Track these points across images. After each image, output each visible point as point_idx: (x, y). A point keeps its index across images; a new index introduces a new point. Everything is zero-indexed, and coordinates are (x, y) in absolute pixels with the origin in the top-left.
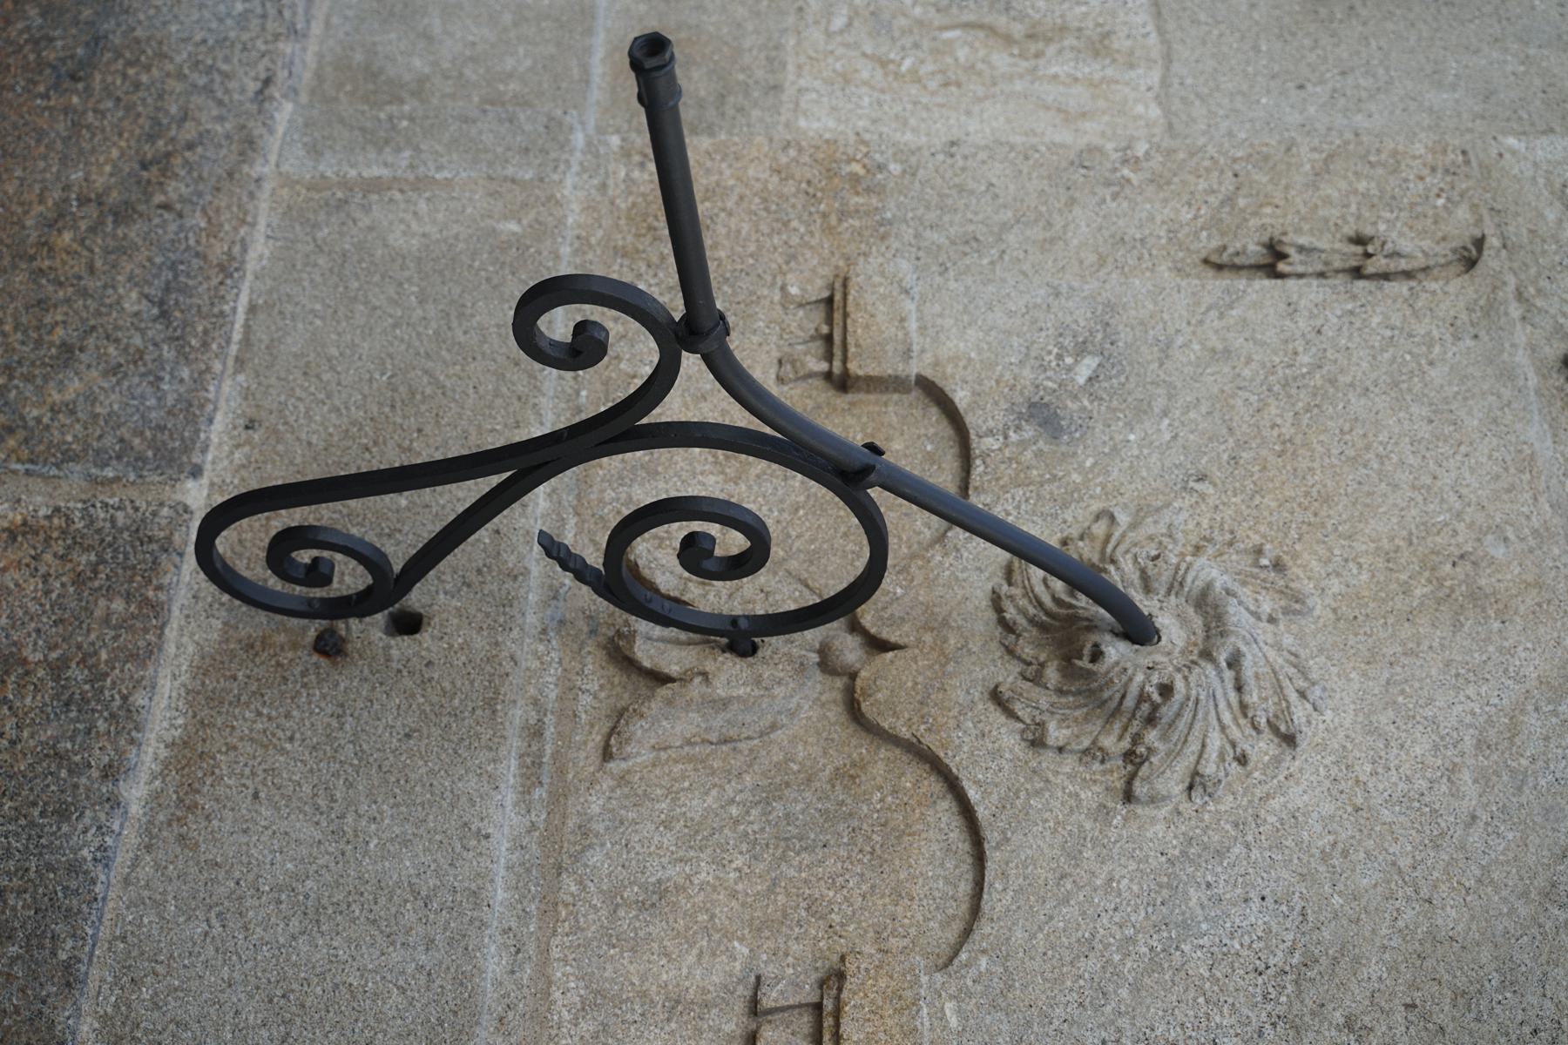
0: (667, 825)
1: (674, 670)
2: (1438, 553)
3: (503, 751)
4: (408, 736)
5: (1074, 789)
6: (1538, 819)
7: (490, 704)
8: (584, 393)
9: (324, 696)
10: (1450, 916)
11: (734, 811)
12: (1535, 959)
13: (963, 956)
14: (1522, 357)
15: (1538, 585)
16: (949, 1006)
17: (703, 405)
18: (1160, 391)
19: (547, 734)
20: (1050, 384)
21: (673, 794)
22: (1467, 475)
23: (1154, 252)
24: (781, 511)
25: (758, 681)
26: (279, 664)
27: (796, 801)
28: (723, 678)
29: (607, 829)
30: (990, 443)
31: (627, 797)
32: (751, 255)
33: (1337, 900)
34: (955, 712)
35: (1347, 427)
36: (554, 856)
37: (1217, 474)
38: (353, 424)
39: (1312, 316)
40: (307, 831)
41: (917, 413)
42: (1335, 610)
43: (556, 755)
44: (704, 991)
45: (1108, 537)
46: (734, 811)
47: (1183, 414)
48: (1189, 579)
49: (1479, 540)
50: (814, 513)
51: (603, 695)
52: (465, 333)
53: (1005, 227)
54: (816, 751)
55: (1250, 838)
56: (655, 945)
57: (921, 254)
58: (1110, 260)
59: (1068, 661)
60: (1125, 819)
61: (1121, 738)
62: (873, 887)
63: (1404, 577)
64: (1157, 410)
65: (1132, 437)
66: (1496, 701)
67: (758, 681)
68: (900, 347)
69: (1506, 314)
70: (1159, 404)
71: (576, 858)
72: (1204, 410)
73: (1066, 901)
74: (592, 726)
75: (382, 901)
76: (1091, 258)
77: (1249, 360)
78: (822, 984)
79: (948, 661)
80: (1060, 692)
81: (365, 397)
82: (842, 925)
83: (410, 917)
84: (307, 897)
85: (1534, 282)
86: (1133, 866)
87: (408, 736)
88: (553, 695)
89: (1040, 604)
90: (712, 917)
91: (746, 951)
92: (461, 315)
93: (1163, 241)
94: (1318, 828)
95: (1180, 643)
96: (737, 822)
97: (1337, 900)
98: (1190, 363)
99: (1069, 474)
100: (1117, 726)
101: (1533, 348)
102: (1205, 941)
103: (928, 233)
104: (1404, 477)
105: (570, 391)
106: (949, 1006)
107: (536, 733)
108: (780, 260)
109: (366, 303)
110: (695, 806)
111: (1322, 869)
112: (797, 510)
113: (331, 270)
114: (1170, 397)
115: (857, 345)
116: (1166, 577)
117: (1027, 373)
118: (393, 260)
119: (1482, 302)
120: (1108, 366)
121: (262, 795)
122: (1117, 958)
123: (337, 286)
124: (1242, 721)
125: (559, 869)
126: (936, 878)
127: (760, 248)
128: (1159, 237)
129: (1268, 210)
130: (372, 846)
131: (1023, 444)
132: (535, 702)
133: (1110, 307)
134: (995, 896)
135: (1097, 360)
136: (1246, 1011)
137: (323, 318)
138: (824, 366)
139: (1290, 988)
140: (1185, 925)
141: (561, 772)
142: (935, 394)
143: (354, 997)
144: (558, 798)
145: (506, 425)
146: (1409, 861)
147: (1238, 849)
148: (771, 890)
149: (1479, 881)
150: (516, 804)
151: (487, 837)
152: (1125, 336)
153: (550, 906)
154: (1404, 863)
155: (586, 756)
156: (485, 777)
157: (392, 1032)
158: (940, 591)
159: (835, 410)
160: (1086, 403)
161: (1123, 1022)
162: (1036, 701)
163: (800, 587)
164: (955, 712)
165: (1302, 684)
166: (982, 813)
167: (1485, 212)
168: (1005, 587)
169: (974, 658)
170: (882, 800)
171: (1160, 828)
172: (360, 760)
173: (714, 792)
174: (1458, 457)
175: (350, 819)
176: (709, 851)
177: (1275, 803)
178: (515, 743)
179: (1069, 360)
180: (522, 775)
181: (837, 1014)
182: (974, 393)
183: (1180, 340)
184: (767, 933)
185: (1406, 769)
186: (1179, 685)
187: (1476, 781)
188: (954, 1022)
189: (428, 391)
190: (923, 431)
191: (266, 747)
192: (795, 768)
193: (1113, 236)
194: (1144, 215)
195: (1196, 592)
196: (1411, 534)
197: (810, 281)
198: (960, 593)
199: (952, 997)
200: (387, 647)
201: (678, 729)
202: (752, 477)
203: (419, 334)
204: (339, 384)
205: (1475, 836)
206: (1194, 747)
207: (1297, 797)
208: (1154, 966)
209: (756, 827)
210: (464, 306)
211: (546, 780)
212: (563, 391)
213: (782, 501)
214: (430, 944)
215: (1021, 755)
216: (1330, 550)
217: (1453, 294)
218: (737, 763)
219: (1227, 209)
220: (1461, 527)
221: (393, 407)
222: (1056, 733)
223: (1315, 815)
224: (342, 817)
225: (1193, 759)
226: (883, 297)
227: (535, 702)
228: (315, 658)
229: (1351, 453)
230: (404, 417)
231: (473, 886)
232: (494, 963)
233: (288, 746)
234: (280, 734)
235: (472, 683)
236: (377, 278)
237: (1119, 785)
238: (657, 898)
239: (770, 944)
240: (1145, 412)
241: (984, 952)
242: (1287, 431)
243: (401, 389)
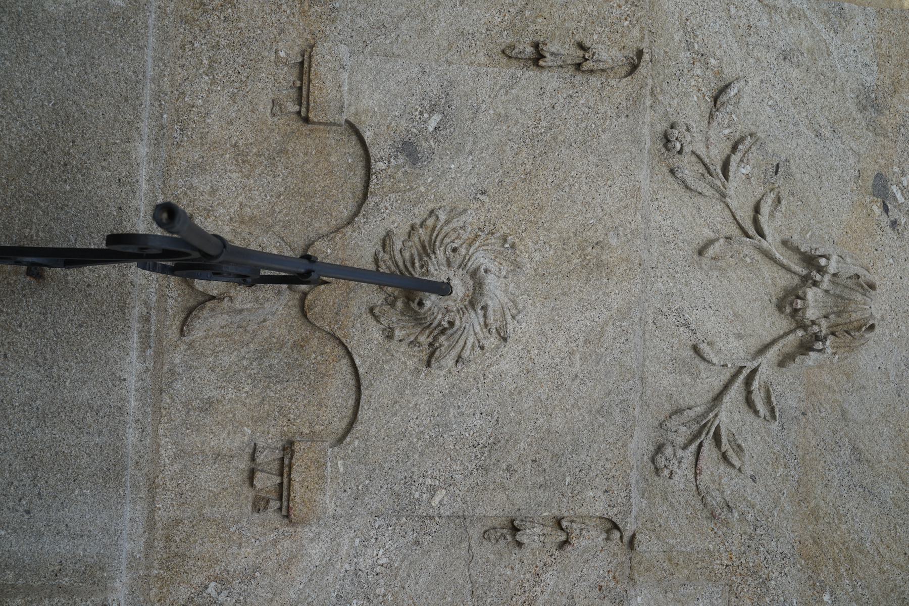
0: (212, 369)
1: (215, 293)
2: (587, 241)
3: (130, 334)
4: (81, 326)
5: (405, 358)
6: (602, 377)
7: (122, 309)
8: (165, 116)
9: (35, 302)
10: (558, 421)
11: (245, 363)
12: (587, 440)
13: (348, 439)
14: (646, 131)
15: (627, 260)
16: (340, 462)
17: (231, 127)
18: (470, 139)
19: (152, 320)
20: (415, 130)
21: (215, 354)
22: (608, 198)
23: (478, 43)
24: (272, 196)
25: (257, 300)
26: (9, 283)
27: (274, 358)
28: (240, 299)
29: (183, 371)
30: (381, 165)
31: (193, 354)
32: (259, 28)
33: (512, 414)
34: (352, 319)
35: (557, 167)
36: (158, 384)
37: (492, 191)
38: (35, 135)
39: (552, 97)
40: (35, 376)
41: (345, 138)
42: (535, 270)
43: (157, 332)
44: (231, 450)
45: (435, 227)
46: (245, 363)
47: (480, 154)
48: (469, 265)
49: (606, 234)
50: (288, 199)
51: (180, 299)
52: (96, 77)
53: (401, 18)
54: (285, 332)
55: (480, 385)
56: (208, 428)
57: (354, 34)
58: (454, 46)
59: (409, 299)
60: (426, 375)
61: (428, 337)
62: (309, 401)
63: (569, 253)
64: (467, 150)
65: (453, 166)
66: (597, 319)
67: (257, 300)
68: (338, 105)
69: (644, 103)
70: (469, 146)
71: (169, 385)
72: (490, 152)
73: (395, 414)
74: (175, 316)
75: (75, 411)
76: (445, 44)
77: (517, 122)
78: (284, 449)
79: (351, 291)
80: (402, 314)
81: (40, 118)
82: (294, 419)
83: (89, 420)
84: (38, 409)
85: (661, 85)
86: (427, 398)
87: (81, 326)
88: (154, 299)
89: (397, 266)
90: (234, 415)
91: (250, 432)
92: (92, 64)
93: (484, 36)
94: (510, 380)
95: (461, 295)
96: (246, 368)
97: (512, 414)
98: (487, 122)
99: (418, 187)
100: (427, 332)
101: (652, 125)
102: (454, 433)
103: (358, 20)
104: (579, 197)
105: (157, 114)
106: (340, 462)
107: (146, 319)
108: (275, 33)
109: (35, 51)
110: (227, 360)
111: (509, 400)
112: (279, 196)
113: (11, 25)
114: (475, 143)
115: (314, 102)
116: (459, 260)
117: (403, 122)
118: (49, 22)
119: (634, 96)
120: (445, 120)
121: (9, 355)
122: (415, 440)
123: (16, 39)
124: (485, 330)
125: (161, 391)
126: (338, 397)
127: (264, 22)
128: (482, 33)
129: (540, 20)
130: (67, 384)
131: (398, 167)
132: (145, 303)
133: (451, 82)
134: (364, 412)
135: (440, 116)
136: (467, 464)
137: (10, 61)
138: (297, 108)
139: (486, 453)
140: (446, 426)
141: (160, 341)
142: (354, 130)
143: (66, 458)
144: (159, 354)
145: (122, 140)
146: (546, 397)
147: (474, 391)
148: (262, 402)
149: (573, 406)
150: (138, 357)
151: (124, 380)
152: (456, 103)
153: (157, 409)
154: (543, 397)
155: (172, 333)
156: (121, 349)
157: (86, 474)
158: (349, 252)
159: (302, 134)
160: (432, 143)
161: (415, 469)
162: (392, 317)
163: (280, 240)
164: (352, 319)
165: (514, 312)
166: (361, 371)
167: (646, 32)
168: (382, 254)
169: (363, 290)
170: (315, 358)
171: (441, 379)
172: (58, 338)
173: (235, 353)
174: (606, 187)
175: (55, 369)
176: (233, 383)
177: (493, 369)
178: (136, 325)
179: (426, 115)
180: (141, 342)
181: (290, 467)
182: (375, 134)
183: (484, 107)
184: (259, 423)
185: (552, 353)
186: (457, 323)
187: (581, 359)
188: (341, 469)
189: (76, 116)
190: (347, 151)
191: (7, 330)
192: (275, 340)
193: (457, 30)
194: (475, 17)
195: (472, 269)
196: (577, 230)
197: (291, 48)
198: (359, 253)
199: (341, 458)
200: (66, 275)
201: (217, 322)
202: (257, 175)
203: (68, 76)
204: (24, 107)
205: (576, 384)
206: (461, 343)
207: (503, 366)
208: (431, 444)
209: (255, 371)
210: (93, 58)
211: (153, 345)
212: (153, 114)
213: (271, 190)
214: (100, 434)
215: (382, 342)
216: (538, 237)
217: (621, 88)
218: (246, 337)
219: (519, 17)
220: (600, 227)
221: (57, 125)
222: (398, 333)
223: (510, 375)
224: (51, 368)
225: (460, 349)
226: (331, 70)
227: (145, 303)
228: (28, 278)
229: (556, 182)
230: (64, 133)
231: (119, 405)
232: (131, 436)
233: (19, 330)
234: (14, 323)
235: (112, 297)
236: (40, 34)
237: (425, 358)
238: (208, 406)
239: (261, 428)
240: (461, 151)
241: (357, 438)
242: (529, 167)
243: (61, 113)
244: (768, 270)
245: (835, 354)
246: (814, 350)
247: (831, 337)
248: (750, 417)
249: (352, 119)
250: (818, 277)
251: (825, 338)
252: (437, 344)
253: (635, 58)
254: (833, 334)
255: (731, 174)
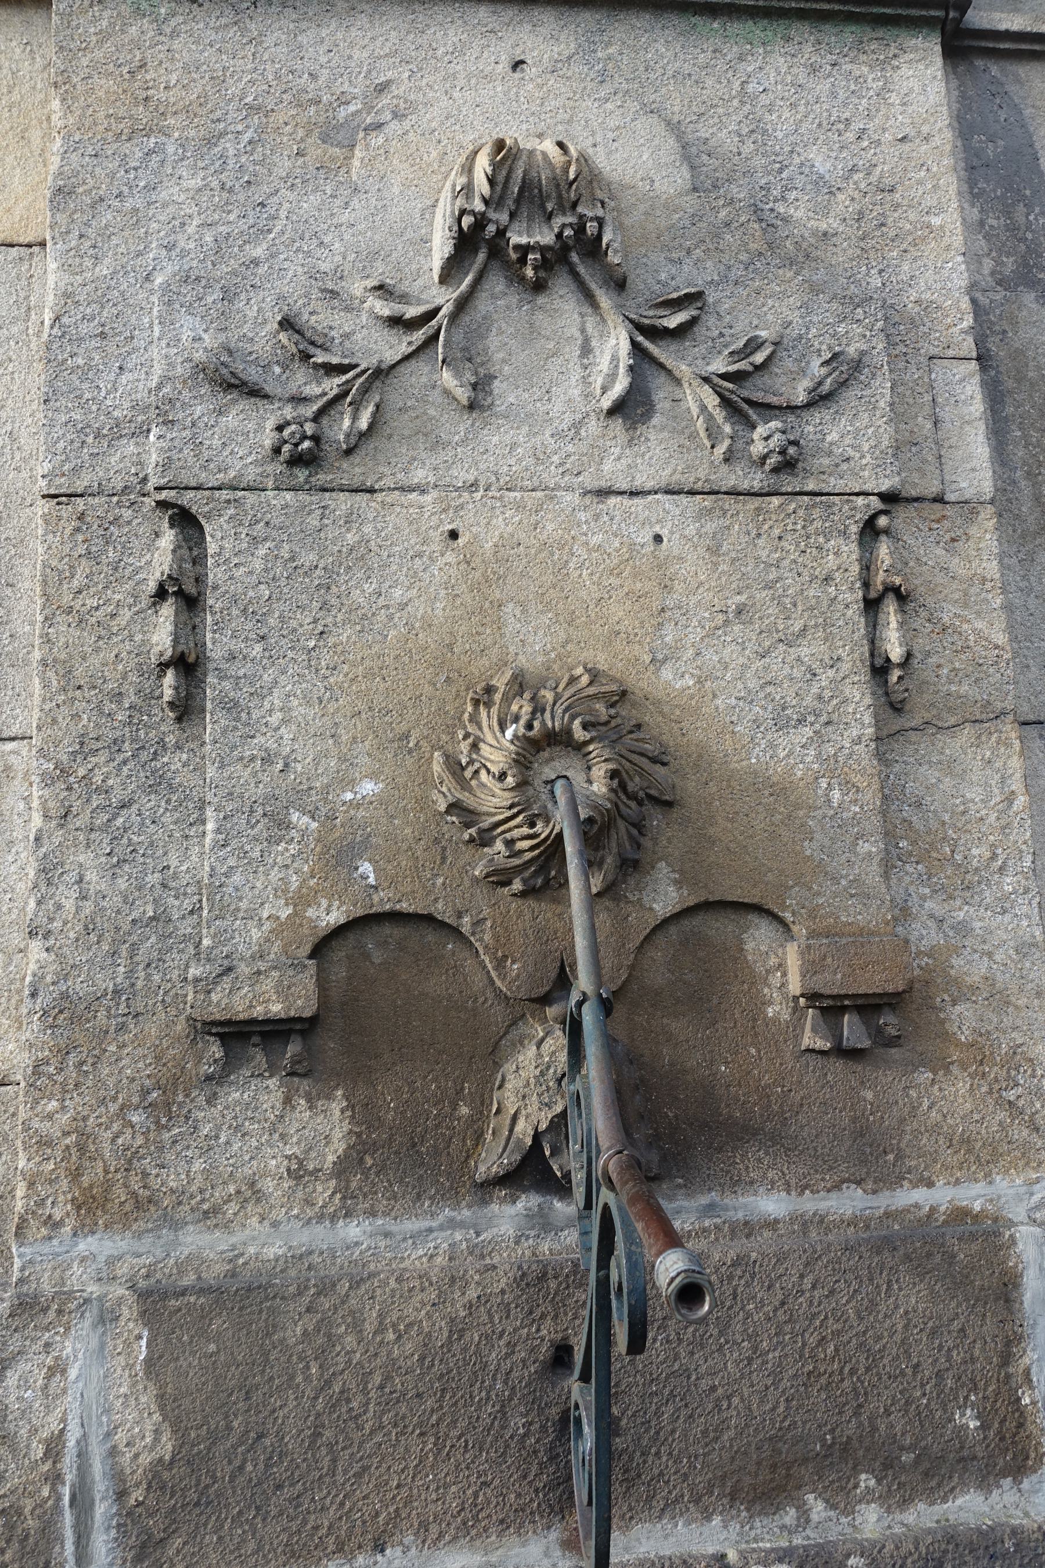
225: (644, 759)
244: (483, 304)
245: (603, 203)
246: (599, 237)
247: (580, 209)
248: (699, 330)
249: (307, 949)
250: (491, 228)
251: (581, 217)
252: (641, 794)
253: (170, 512)
254: (574, 205)
255: (346, 361)
